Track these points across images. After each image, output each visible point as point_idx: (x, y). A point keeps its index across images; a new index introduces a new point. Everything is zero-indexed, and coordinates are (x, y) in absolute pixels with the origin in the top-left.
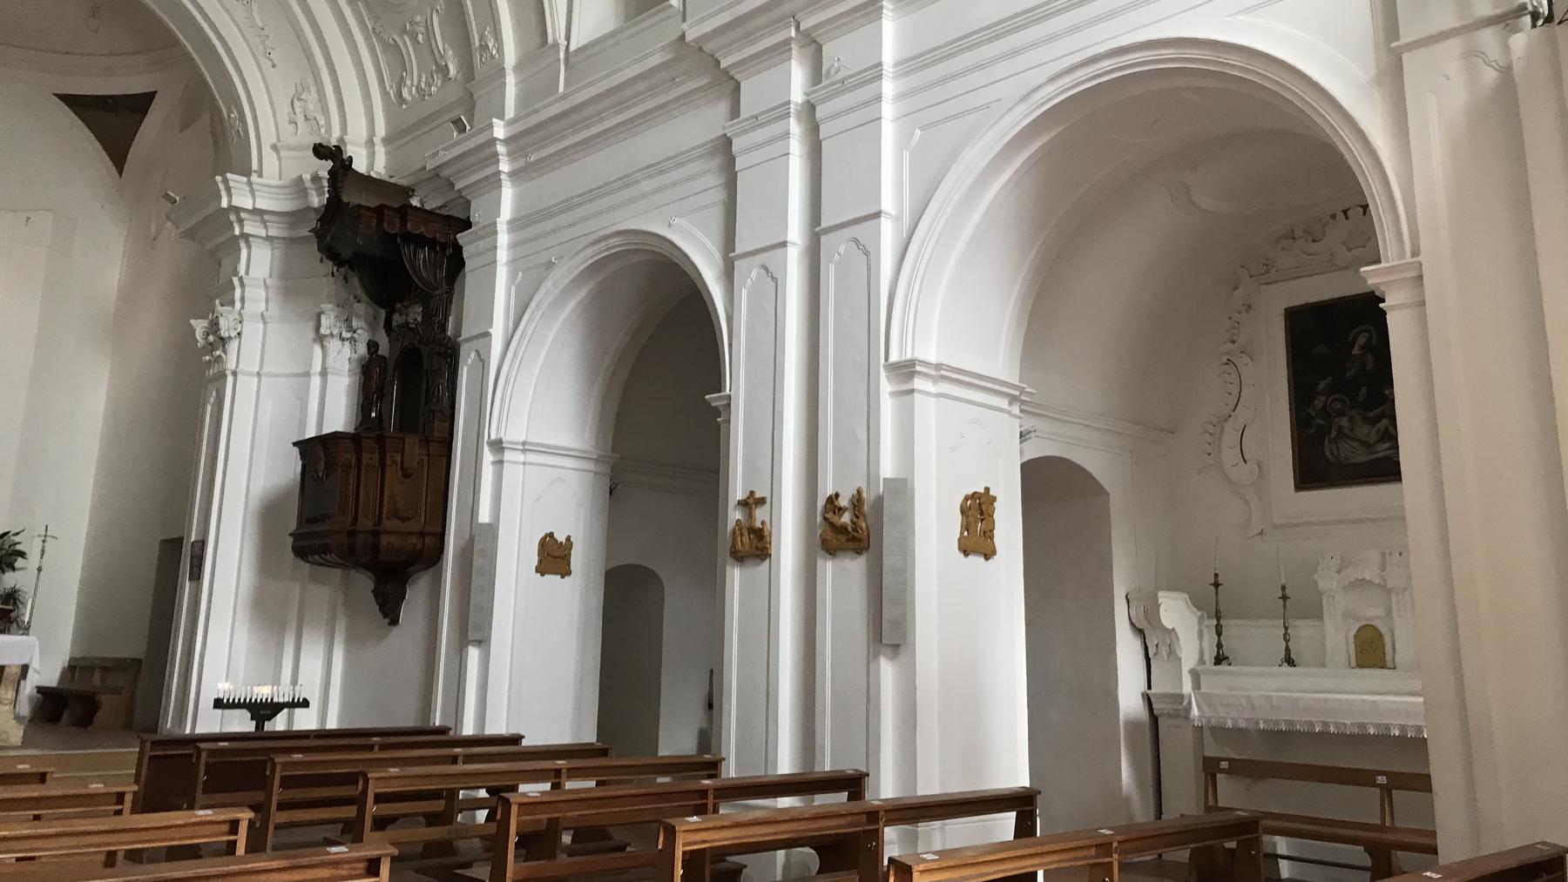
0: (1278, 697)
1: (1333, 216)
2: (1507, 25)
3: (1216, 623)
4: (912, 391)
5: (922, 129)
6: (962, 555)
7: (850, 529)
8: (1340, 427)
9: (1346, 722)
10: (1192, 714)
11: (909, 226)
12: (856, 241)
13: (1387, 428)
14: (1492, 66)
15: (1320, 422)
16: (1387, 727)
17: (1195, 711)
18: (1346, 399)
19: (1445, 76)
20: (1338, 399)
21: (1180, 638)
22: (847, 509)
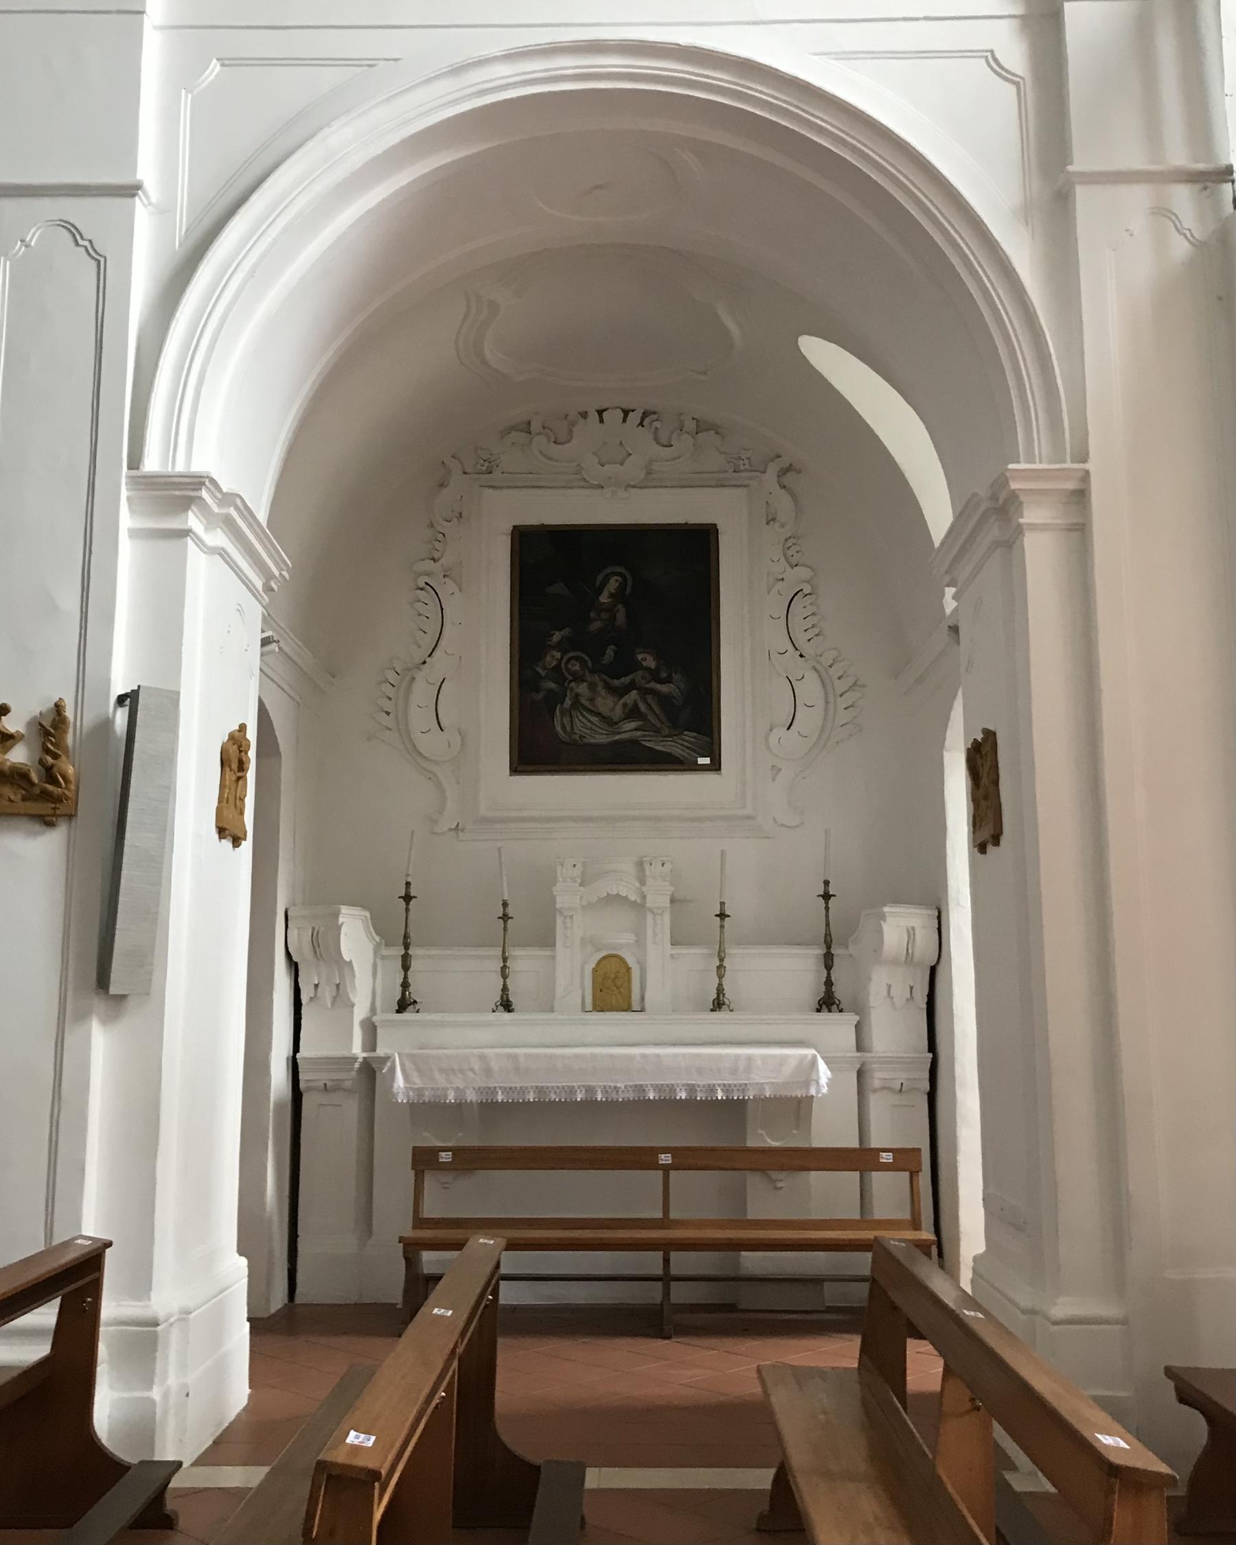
0: (527, 1056)
1: (584, 415)
2: (1205, 188)
3: (403, 952)
4: (186, 533)
5: (223, 62)
6: (217, 836)
7: (35, 777)
8: (577, 695)
9: (619, 1085)
10: (396, 1086)
11: (186, 237)
12: (74, 232)
13: (636, 704)
14: (1186, 236)
15: (552, 685)
16: (672, 1089)
17: (400, 1081)
18: (587, 658)
19: (1127, 230)
20: (576, 658)
21: (357, 974)
22: (23, 736)
